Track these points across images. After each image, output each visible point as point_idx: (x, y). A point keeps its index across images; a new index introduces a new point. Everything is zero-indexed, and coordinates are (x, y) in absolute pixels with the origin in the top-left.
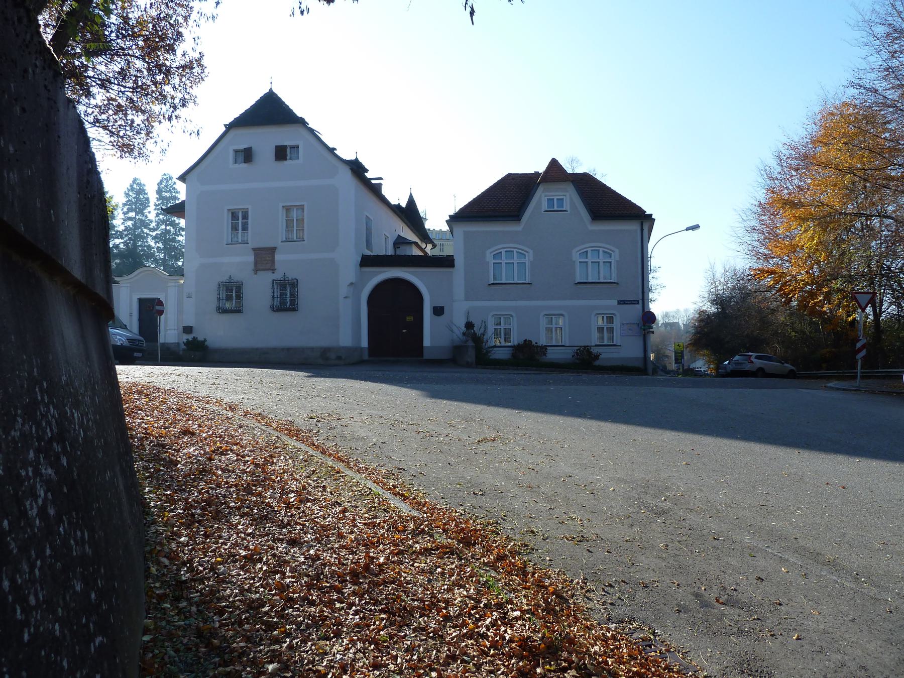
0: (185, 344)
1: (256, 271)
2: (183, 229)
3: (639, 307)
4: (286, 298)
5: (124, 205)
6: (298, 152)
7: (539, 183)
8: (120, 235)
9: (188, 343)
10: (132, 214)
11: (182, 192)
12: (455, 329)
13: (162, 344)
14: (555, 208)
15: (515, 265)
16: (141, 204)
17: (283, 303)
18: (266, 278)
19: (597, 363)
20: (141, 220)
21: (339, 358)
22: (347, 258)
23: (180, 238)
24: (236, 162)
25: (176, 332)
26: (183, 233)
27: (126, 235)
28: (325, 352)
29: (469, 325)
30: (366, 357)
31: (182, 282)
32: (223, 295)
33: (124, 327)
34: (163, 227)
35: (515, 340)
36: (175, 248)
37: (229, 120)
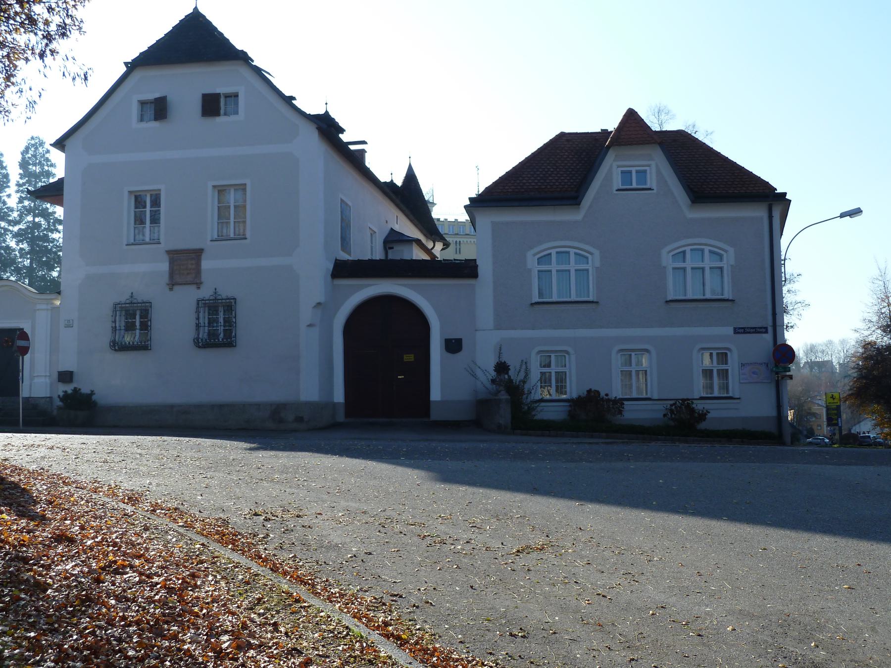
1: (172, 284)
2: (60, 222)
3: (768, 337)
4: (218, 327)
6: (237, 104)
7: (609, 147)
9: (66, 398)
11: (58, 165)
12: (479, 373)
13: (27, 400)
14: (634, 186)
17: (213, 334)
18: (187, 298)
19: (702, 426)
21: (299, 419)
23: (55, 236)
24: (142, 119)
25: (48, 380)
26: (60, 227)
29: (502, 368)
30: (341, 417)
31: (58, 303)
32: (121, 323)
34: (30, 218)
35: (573, 390)
37: (132, 54)
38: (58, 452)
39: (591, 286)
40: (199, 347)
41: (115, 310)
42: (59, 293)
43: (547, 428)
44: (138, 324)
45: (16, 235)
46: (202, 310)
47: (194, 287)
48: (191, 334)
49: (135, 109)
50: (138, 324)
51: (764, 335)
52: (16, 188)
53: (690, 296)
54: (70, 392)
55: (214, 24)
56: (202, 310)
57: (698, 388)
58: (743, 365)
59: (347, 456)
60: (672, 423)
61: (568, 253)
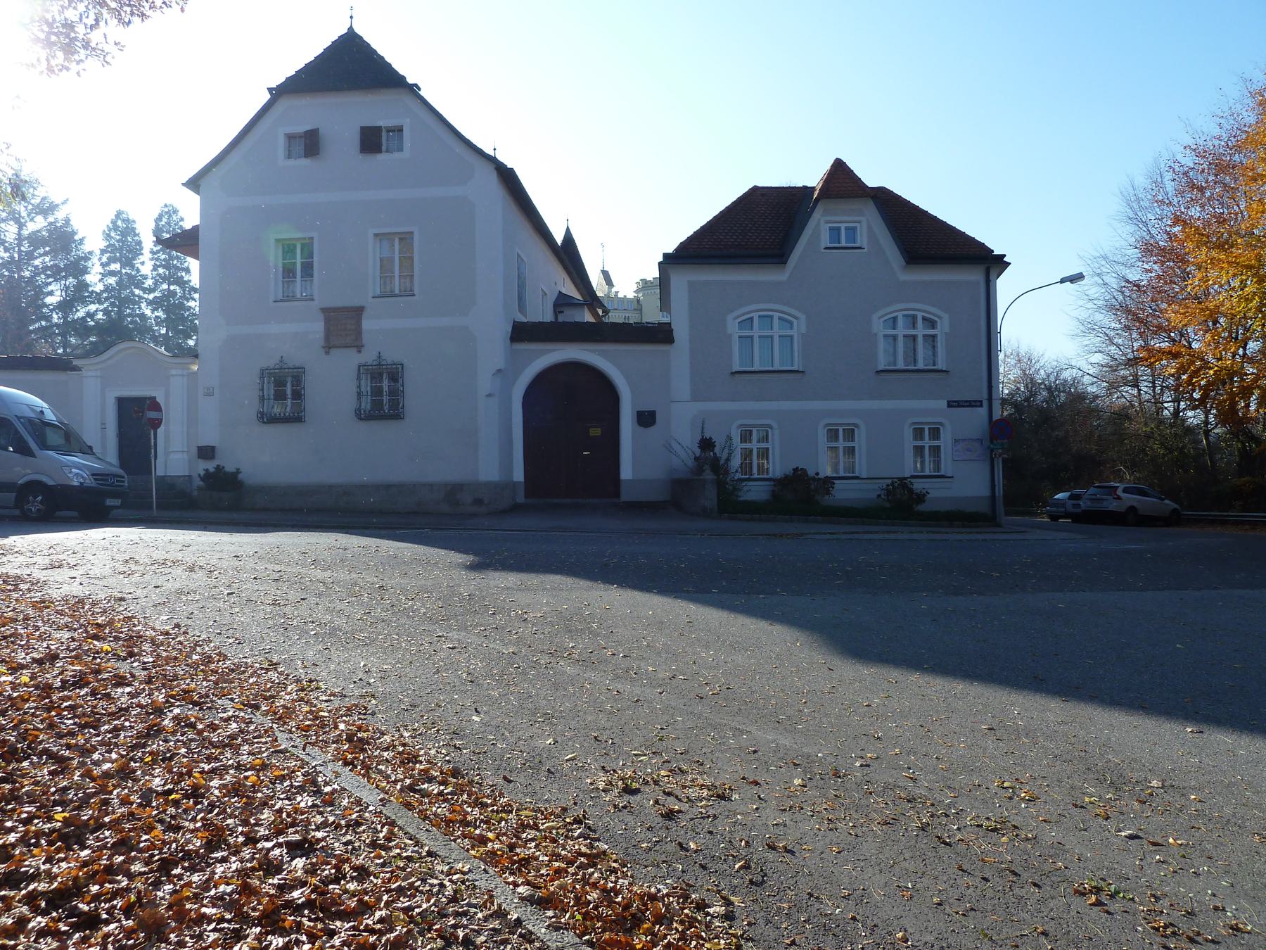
0: (202, 479)
1: (328, 347)
2: (195, 290)
3: (983, 411)
4: (383, 396)
5: (103, 252)
6: (401, 139)
7: (817, 200)
8: (97, 298)
9: (207, 477)
10: (115, 267)
11: (190, 212)
12: (676, 447)
13: (161, 480)
14: (843, 244)
15: (756, 340)
16: (130, 251)
17: (377, 404)
18: (346, 364)
19: (921, 508)
20: (130, 276)
21: (478, 502)
22: (490, 323)
23: (192, 304)
24: (289, 157)
25: (185, 456)
26: (196, 296)
27: (107, 299)
28: (453, 491)
29: (706, 444)
30: (521, 499)
31: (195, 368)
32: (270, 390)
33: (87, 450)
34: (165, 286)
35: (777, 467)
36: (184, 319)
37: (277, 80)
38: (200, 575)
39: (796, 354)
40: (361, 419)
41: (262, 376)
42: (196, 356)
43: (753, 510)
44: (289, 392)
45: (150, 303)
46: (363, 376)
47: (353, 351)
48: (350, 403)
49: (281, 141)
50: (289, 392)
51: (979, 409)
52: (150, 256)
53: (756, 367)
54: (212, 470)
55: (373, 46)
56: (363, 376)
57: (908, 466)
58: (956, 441)
59: (620, 585)
60: (887, 505)
61: (771, 317)
